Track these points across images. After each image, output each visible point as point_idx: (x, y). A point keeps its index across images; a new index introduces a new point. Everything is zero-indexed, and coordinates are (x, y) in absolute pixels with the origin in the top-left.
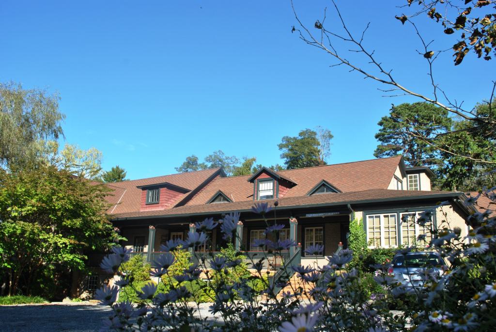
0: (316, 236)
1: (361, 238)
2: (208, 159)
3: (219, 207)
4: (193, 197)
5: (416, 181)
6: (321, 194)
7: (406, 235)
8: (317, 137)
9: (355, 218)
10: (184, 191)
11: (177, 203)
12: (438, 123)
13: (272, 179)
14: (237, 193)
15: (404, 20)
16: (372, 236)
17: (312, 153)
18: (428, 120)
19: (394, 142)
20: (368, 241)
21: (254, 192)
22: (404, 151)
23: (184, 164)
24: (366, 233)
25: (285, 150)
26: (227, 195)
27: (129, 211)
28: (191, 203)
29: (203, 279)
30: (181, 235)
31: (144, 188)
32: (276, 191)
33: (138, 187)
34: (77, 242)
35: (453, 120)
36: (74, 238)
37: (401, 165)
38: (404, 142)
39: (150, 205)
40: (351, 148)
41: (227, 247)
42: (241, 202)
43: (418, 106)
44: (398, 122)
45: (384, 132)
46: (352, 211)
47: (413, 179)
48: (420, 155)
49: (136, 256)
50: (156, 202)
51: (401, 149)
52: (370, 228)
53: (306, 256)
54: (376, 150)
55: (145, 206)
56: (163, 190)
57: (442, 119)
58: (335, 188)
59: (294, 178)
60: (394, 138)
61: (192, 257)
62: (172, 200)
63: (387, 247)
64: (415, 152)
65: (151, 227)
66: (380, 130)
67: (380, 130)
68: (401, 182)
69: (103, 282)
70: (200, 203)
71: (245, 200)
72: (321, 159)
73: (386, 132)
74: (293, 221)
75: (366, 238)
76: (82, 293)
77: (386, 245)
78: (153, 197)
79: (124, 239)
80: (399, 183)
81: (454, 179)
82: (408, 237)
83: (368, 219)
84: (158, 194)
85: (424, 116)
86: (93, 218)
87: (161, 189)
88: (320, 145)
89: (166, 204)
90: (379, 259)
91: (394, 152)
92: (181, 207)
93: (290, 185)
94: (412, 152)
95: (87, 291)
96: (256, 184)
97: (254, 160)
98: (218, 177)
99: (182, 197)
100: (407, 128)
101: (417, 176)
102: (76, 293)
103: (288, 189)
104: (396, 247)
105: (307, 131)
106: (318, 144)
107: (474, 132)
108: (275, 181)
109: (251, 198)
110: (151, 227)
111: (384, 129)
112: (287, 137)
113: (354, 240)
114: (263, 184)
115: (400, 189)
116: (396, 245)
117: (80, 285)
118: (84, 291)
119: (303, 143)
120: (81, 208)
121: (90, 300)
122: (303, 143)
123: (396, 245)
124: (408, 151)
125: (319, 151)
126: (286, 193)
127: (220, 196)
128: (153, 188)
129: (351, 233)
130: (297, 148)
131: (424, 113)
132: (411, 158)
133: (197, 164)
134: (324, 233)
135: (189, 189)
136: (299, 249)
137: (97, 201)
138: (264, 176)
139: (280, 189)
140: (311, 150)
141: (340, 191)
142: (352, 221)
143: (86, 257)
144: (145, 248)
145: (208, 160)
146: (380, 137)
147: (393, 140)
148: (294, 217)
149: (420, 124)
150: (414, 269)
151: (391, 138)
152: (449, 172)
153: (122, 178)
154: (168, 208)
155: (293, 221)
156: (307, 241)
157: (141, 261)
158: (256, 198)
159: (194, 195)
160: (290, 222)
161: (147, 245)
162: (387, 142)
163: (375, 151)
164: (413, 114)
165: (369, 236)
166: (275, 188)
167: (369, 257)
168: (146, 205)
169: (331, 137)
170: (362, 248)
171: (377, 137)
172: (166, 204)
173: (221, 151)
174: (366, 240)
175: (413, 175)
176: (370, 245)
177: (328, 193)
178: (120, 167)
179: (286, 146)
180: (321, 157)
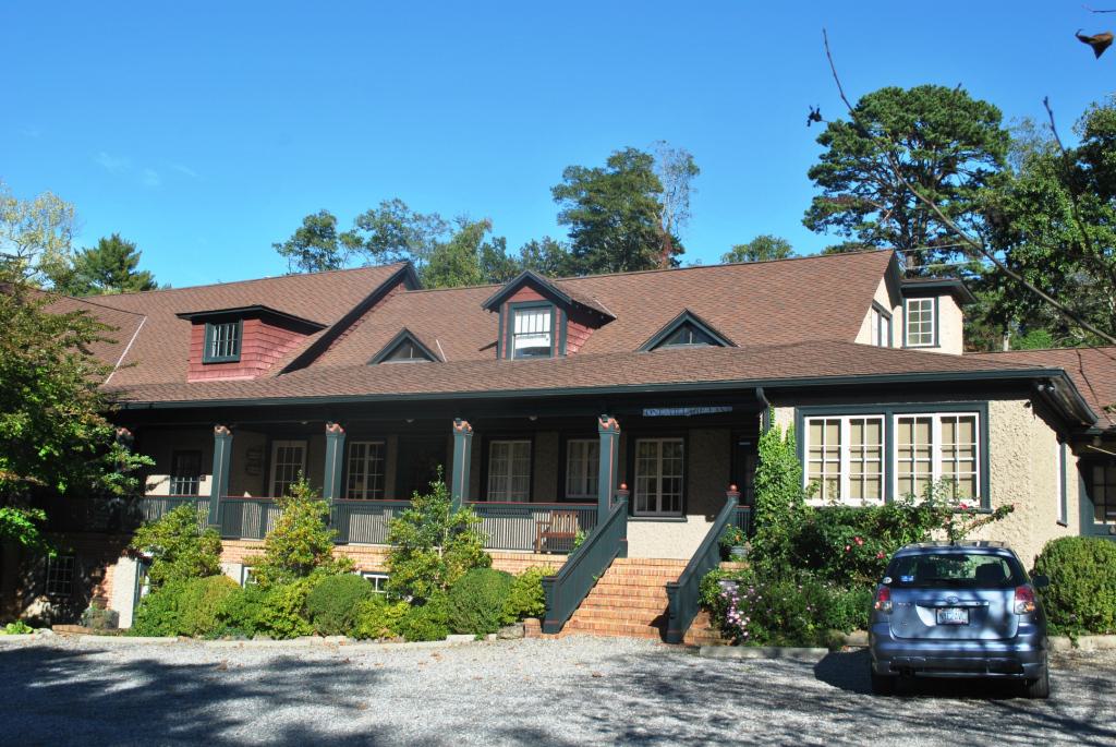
0: (664, 462)
1: (787, 478)
2: (364, 221)
3: (407, 380)
4: (331, 343)
5: (926, 316)
6: (680, 348)
7: (908, 474)
8: (655, 170)
9: (776, 424)
10: (306, 327)
11: (290, 361)
12: (974, 144)
13: (550, 303)
14: (452, 335)
15: (1100, 46)
16: (817, 474)
17: (642, 213)
18: (949, 135)
19: (856, 190)
20: (805, 486)
21: (501, 337)
22: (883, 214)
23: (298, 233)
24: (801, 464)
25: (571, 204)
26: (425, 343)
27: (157, 380)
28: (326, 361)
29: (363, 573)
30: (299, 450)
31: (197, 319)
32: (559, 334)
33: (180, 316)
34: (16, 478)
35: (1012, 136)
36: (8, 465)
37: (891, 275)
38: (882, 191)
39: (215, 367)
40: (747, 201)
41: (431, 491)
42: (464, 362)
43: (924, 98)
44: (869, 137)
45: (833, 162)
46: (766, 406)
47: (920, 311)
48: (924, 226)
49: (180, 510)
50: (230, 356)
51: (873, 209)
52: (811, 451)
53: (636, 512)
54: (808, 209)
55: (202, 368)
56: (250, 327)
57: (985, 133)
58: (718, 334)
59: (606, 299)
60: (857, 180)
61: (333, 512)
62: (275, 354)
63: (856, 503)
64: (910, 217)
65: (220, 430)
66: (822, 157)
67: (822, 157)
68: (889, 319)
69: (88, 574)
70: (350, 372)
71: (475, 358)
72: (665, 228)
73: (838, 163)
74: (608, 424)
75: (802, 477)
76: (31, 602)
77: (852, 497)
78: (222, 344)
79: (146, 459)
80: (883, 319)
81: (1018, 304)
82: (912, 478)
83: (809, 431)
84: (236, 336)
85: (947, 123)
86: (59, 407)
87: (245, 323)
88: (662, 191)
89: (260, 365)
90: (836, 537)
91: (854, 215)
92: (300, 371)
93: (595, 319)
94: (903, 220)
95: (44, 598)
96: (506, 316)
97: (487, 225)
98: (400, 289)
99: (302, 344)
100: (894, 154)
101: (930, 302)
102: (14, 603)
103: (591, 331)
104: (881, 503)
105: (629, 154)
106: (659, 190)
107: (1075, 182)
108: (558, 310)
109: (491, 353)
110: (220, 430)
111: (833, 154)
112: (578, 168)
113: (770, 481)
114: (526, 318)
115: (885, 344)
116: (880, 497)
117: (26, 580)
118: (35, 597)
119: (617, 186)
120: (26, 380)
121: (54, 627)
122: (617, 186)
123: (880, 497)
124: (892, 216)
125: (660, 207)
126: (585, 341)
127: (406, 344)
128: (225, 321)
129: (761, 464)
130: (600, 199)
131: (941, 114)
132: (898, 232)
133: (333, 233)
134: (686, 448)
135: (321, 321)
136: (622, 501)
137: (70, 360)
138: (526, 294)
139: (570, 331)
140: (640, 204)
141: (731, 344)
142: (765, 433)
143: (42, 515)
144: (202, 484)
145: (363, 223)
146: (821, 176)
147: (854, 185)
148: (610, 416)
149: (928, 145)
150: (949, 595)
151: (850, 177)
152: (1004, 284)
153: (130, 267)
154: (265, 376)
155: (608, 424)
156: (640, 474)
157: (194, 521)
158: (503, 355)
159: (336, 337)
160: (600, 429)
161: (210, 473)
162: (838, 188)
163: (807, 213)
164: (912, 117)
165: (809, 471)
166: (558, 328)
167: (809, 530)
168: (204, 364)
169: (692, 170)
170: (791, 504)
171: (813, 174)
172: (260, 365)
173: (400, 202)
174: (803, 482)
175: (920, 300)
176: (811, 496)
177: (697, 346)
178: (123, 238)
179: (574, 192)
180: (664, 223)
